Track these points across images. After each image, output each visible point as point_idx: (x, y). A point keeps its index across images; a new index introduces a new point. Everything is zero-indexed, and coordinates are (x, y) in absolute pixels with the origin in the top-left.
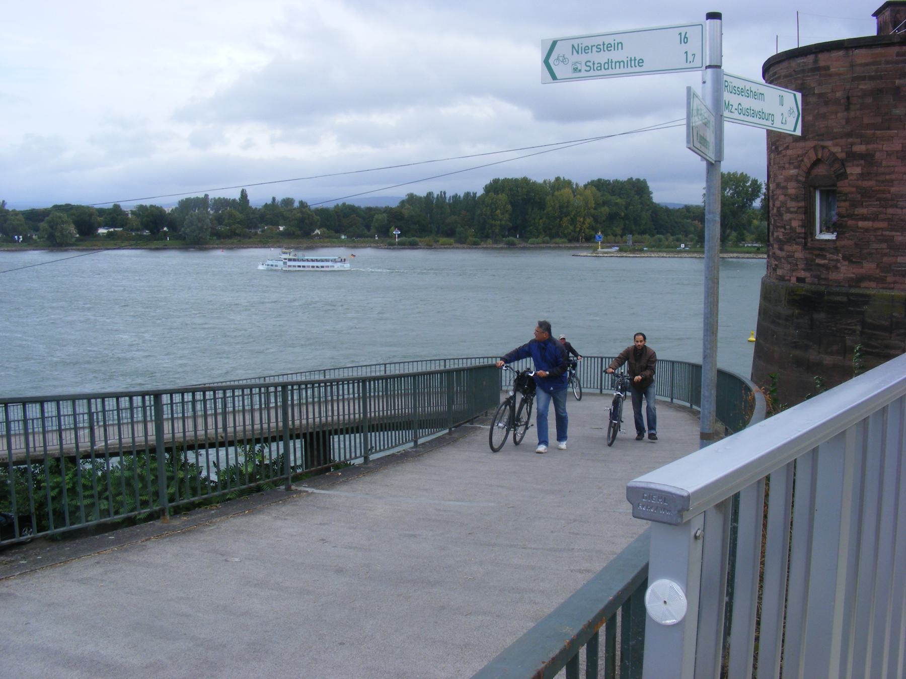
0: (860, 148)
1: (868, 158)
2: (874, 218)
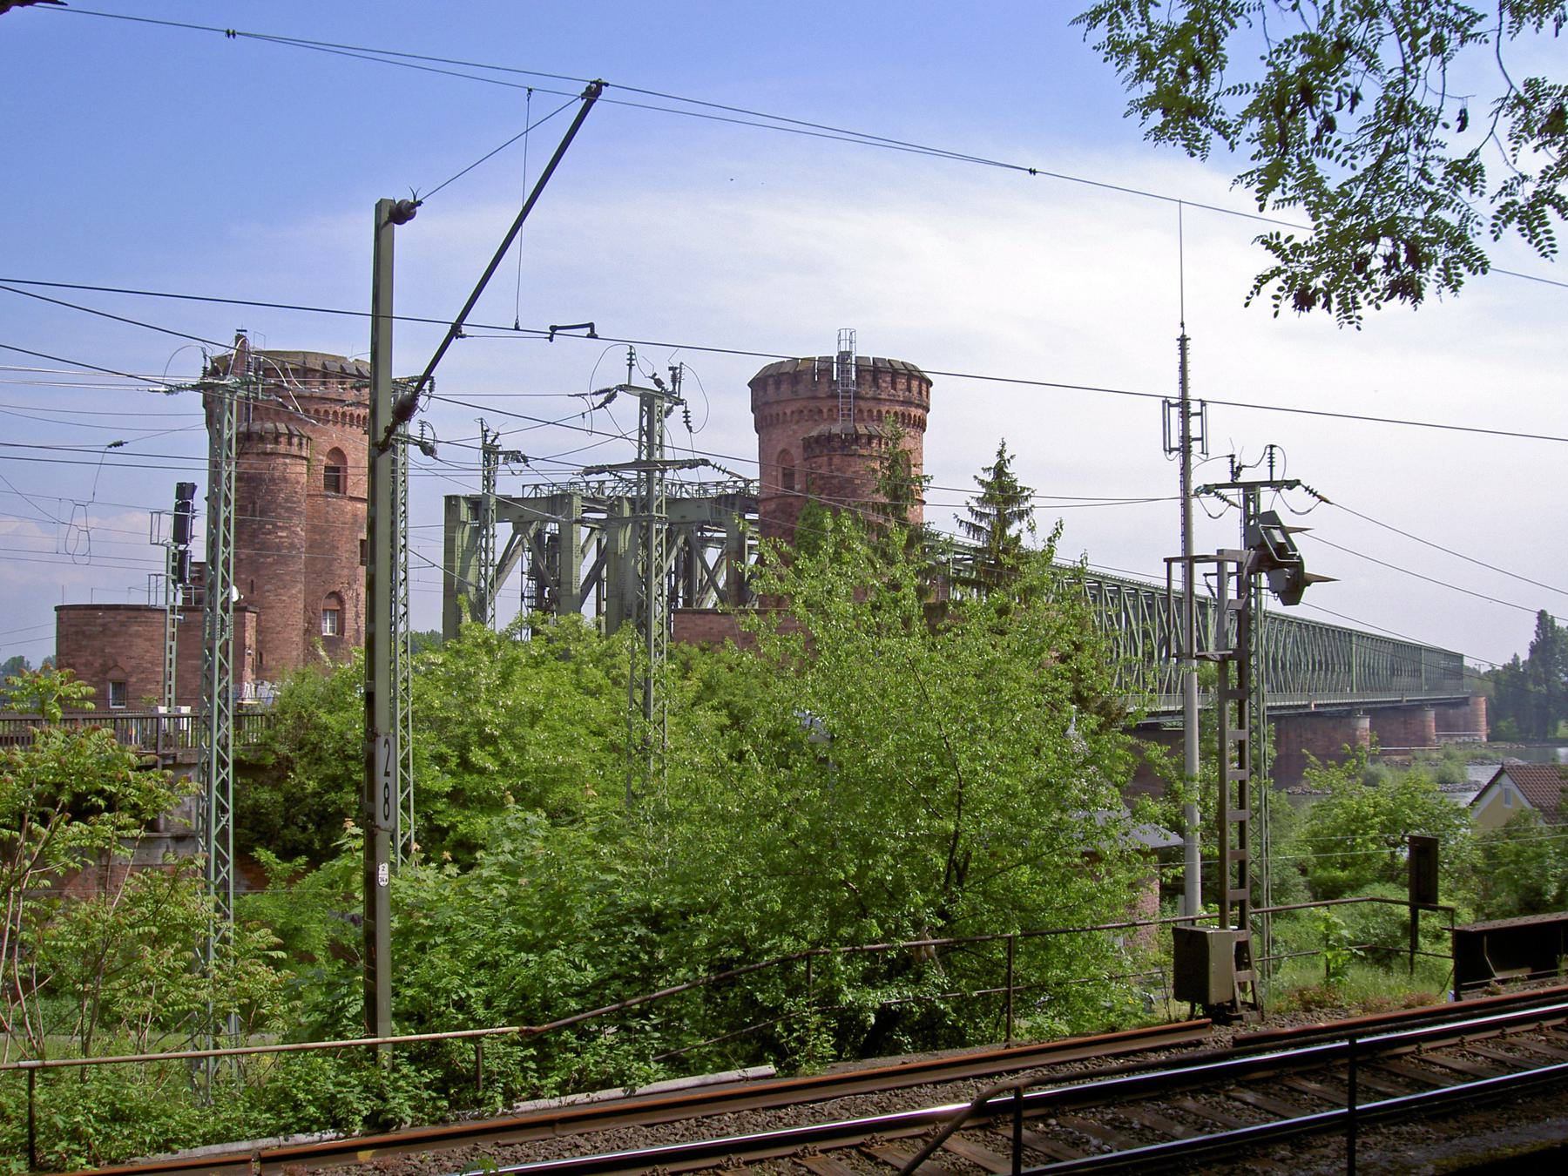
0: (71, 661)
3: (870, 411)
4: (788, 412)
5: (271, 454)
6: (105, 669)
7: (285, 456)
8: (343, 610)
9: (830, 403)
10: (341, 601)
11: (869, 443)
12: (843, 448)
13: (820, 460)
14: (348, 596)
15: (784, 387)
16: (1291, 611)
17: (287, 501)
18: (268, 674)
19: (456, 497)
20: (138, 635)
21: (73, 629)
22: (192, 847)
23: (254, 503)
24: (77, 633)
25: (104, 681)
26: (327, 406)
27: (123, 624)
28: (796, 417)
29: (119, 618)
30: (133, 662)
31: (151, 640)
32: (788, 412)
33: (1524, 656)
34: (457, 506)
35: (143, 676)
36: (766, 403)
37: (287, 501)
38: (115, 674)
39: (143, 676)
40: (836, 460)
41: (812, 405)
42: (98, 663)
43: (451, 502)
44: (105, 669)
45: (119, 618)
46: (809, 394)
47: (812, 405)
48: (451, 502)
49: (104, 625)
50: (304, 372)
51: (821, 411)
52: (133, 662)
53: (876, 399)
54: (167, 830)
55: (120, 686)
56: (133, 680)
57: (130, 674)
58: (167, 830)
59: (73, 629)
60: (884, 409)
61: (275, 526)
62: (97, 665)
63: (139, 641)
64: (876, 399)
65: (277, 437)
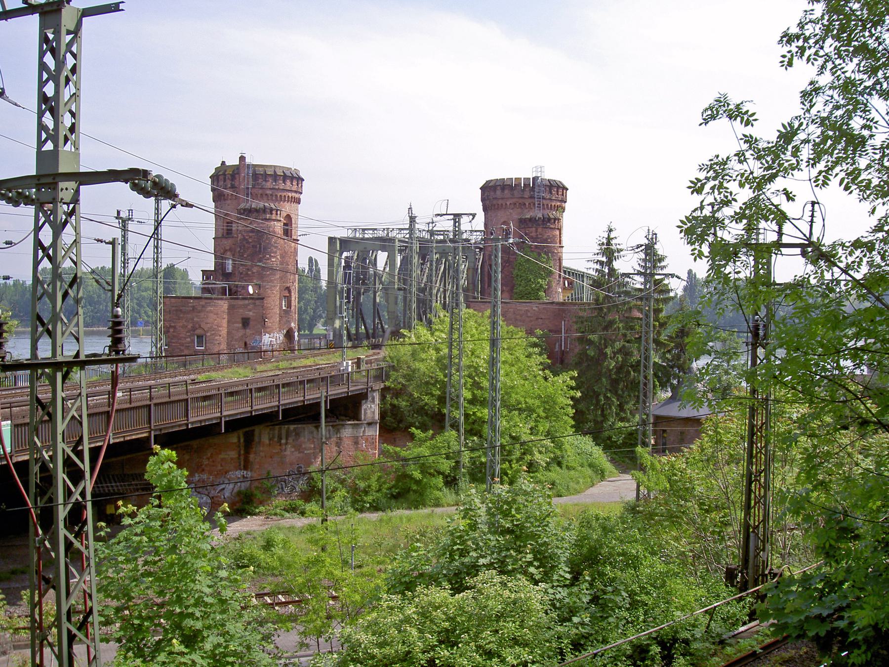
0: (173, 324)
1: (174, 327)
2: (176, 343)
3: (547, 205)
4: (508, 203)
5: (269, 219)
6: (194, 329)
7: (274, 220)
8: (291, 295)
9: (530, 201)
10: (290, 292)
11: (555, 222)
12: (543, 224)
13: (531, 229)
14: (292, 288)
15: (506, 192)
16: (397, 252)
17: (275, 243)
18: (268, 330)
19: (335, 238)
20: (211, 312)
21: (174, 308)
22: (374, 429)
23: (260, 244)
24: (177, 310)
25: (194, 335)
26: (285, 194)
27: (203, 306)
28: (513, 206)
29: (201, 303)
30: (209, 326)
31: (217, 314)
32: (508, 203)
33: (22, 205)
34: (335, 242)
35: (213, 332)
36: (496, 198)
37: (275, 243)
38: (199, 332)
39: (213, 332)
40: (540, 230)
41: (521, 201)
42: (190, 326)
43: (332, 240)
44: (194, 329)
45: (201, 303)
46: (520, 196)
47: (521, 201)
48: (332, 240)
49: (193, 307)
50: (275, 177)
51: (525, 204)
52: (209, 326)
53: (550, 199)
54: (365, 420)
55: (200, 337)
56: (208, 334)
57: (207, 332)
58: (365, 420)
59: (174, 308)
60: (553, 204)
61: (270, 256)
62: (189, 327)
63: (211, 315)
64: (550, 199)
65: (271, 210)
